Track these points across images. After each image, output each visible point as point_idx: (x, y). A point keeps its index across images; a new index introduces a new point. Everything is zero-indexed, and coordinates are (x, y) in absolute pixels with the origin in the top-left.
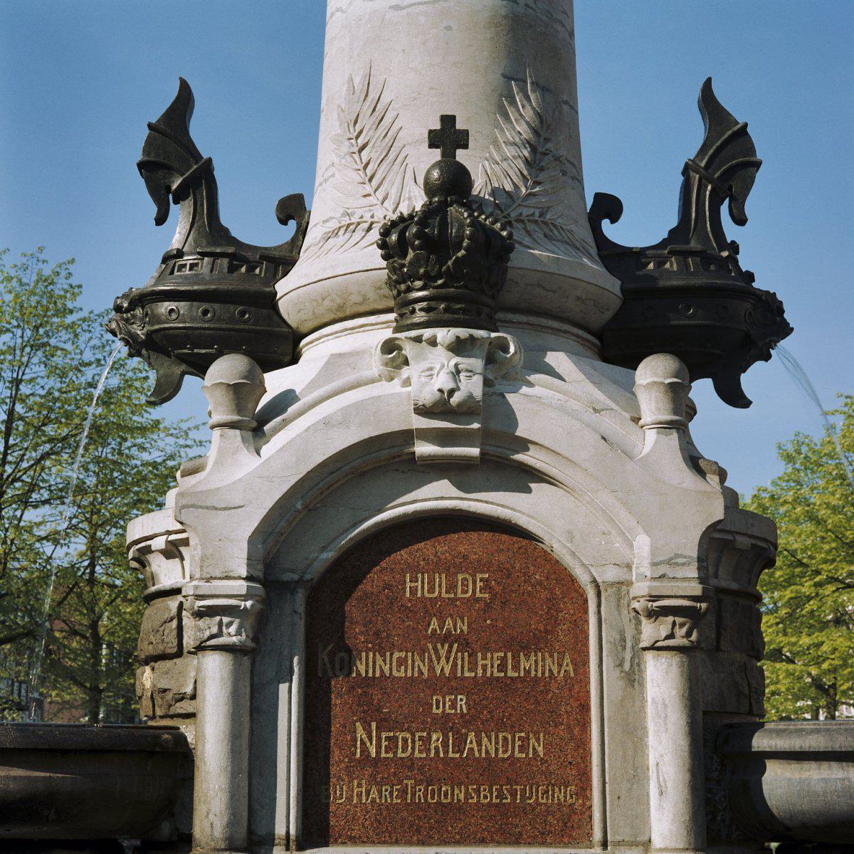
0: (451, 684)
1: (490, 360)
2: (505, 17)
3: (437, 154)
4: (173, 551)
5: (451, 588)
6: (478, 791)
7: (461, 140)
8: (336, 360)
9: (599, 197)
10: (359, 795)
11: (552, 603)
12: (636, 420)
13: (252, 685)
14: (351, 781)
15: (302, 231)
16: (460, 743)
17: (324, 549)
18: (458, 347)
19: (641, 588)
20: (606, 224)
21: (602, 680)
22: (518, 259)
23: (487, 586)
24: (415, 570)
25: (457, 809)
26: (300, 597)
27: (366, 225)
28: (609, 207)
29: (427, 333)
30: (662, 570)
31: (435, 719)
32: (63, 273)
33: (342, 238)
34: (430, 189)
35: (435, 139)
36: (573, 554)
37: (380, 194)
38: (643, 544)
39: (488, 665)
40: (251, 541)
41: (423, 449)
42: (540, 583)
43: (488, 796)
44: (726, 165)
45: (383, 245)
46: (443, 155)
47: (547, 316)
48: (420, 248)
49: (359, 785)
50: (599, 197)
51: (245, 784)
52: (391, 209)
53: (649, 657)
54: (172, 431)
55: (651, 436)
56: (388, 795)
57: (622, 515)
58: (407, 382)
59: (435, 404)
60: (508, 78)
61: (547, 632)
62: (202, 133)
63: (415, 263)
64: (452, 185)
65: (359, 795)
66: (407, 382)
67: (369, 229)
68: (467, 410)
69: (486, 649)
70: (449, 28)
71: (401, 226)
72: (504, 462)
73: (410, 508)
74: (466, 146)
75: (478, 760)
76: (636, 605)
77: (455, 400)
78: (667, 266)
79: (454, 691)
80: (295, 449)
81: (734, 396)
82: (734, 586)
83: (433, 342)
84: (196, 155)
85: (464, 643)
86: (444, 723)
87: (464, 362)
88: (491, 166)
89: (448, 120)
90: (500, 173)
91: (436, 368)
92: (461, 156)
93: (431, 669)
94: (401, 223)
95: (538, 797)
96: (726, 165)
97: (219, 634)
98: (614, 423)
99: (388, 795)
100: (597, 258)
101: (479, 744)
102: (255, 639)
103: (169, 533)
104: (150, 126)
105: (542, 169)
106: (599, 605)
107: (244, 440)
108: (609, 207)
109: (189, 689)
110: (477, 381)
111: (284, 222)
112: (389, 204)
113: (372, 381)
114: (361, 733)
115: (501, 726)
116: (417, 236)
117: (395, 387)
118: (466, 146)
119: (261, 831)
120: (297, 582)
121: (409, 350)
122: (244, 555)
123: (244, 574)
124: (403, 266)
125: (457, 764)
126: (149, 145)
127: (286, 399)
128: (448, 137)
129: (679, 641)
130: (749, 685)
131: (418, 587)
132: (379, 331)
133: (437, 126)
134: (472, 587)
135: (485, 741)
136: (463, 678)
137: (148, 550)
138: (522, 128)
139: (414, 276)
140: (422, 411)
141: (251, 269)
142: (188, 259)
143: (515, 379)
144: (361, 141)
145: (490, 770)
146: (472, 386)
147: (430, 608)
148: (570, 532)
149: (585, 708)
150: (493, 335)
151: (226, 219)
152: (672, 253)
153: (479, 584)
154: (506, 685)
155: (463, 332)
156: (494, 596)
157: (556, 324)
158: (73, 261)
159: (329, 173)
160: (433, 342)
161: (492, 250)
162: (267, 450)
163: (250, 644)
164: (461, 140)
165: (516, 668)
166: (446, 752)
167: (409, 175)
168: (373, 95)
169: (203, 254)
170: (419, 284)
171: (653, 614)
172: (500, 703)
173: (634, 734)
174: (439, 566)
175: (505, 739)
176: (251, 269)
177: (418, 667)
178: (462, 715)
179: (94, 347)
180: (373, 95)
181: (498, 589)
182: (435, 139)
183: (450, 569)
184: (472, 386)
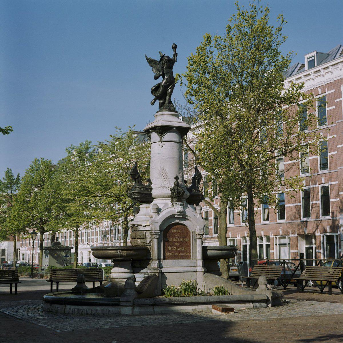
0: (177, 242)
7: (178, 178)
11: (187, 233)
18: (181, 205)
23: (181, 231)
24: (173, 229)
38: (198, 227)
39: (181, 240)
43: (181, 254)
55: (198, 215)
56: (171, 254)
68: (182, 212)
73: (183, 223)
83: (178, 204)
85: (178, 237)
86: (176, 246)
89: (177, 176)
98: (194, 213)
99: (171, 254)
114: (168, 247)
117: (173, 209)
121: (175, 205)
134: (179, 231)
144: (163, 175)
147: (175, 233)
154: (182, 242)
155: (181, 203)
160: (178, 204)
168: (164, 170)
171: (199, 235)
177: (174, 240)
180: (164, 170)
183: (177, 229)
184: (182, 210)
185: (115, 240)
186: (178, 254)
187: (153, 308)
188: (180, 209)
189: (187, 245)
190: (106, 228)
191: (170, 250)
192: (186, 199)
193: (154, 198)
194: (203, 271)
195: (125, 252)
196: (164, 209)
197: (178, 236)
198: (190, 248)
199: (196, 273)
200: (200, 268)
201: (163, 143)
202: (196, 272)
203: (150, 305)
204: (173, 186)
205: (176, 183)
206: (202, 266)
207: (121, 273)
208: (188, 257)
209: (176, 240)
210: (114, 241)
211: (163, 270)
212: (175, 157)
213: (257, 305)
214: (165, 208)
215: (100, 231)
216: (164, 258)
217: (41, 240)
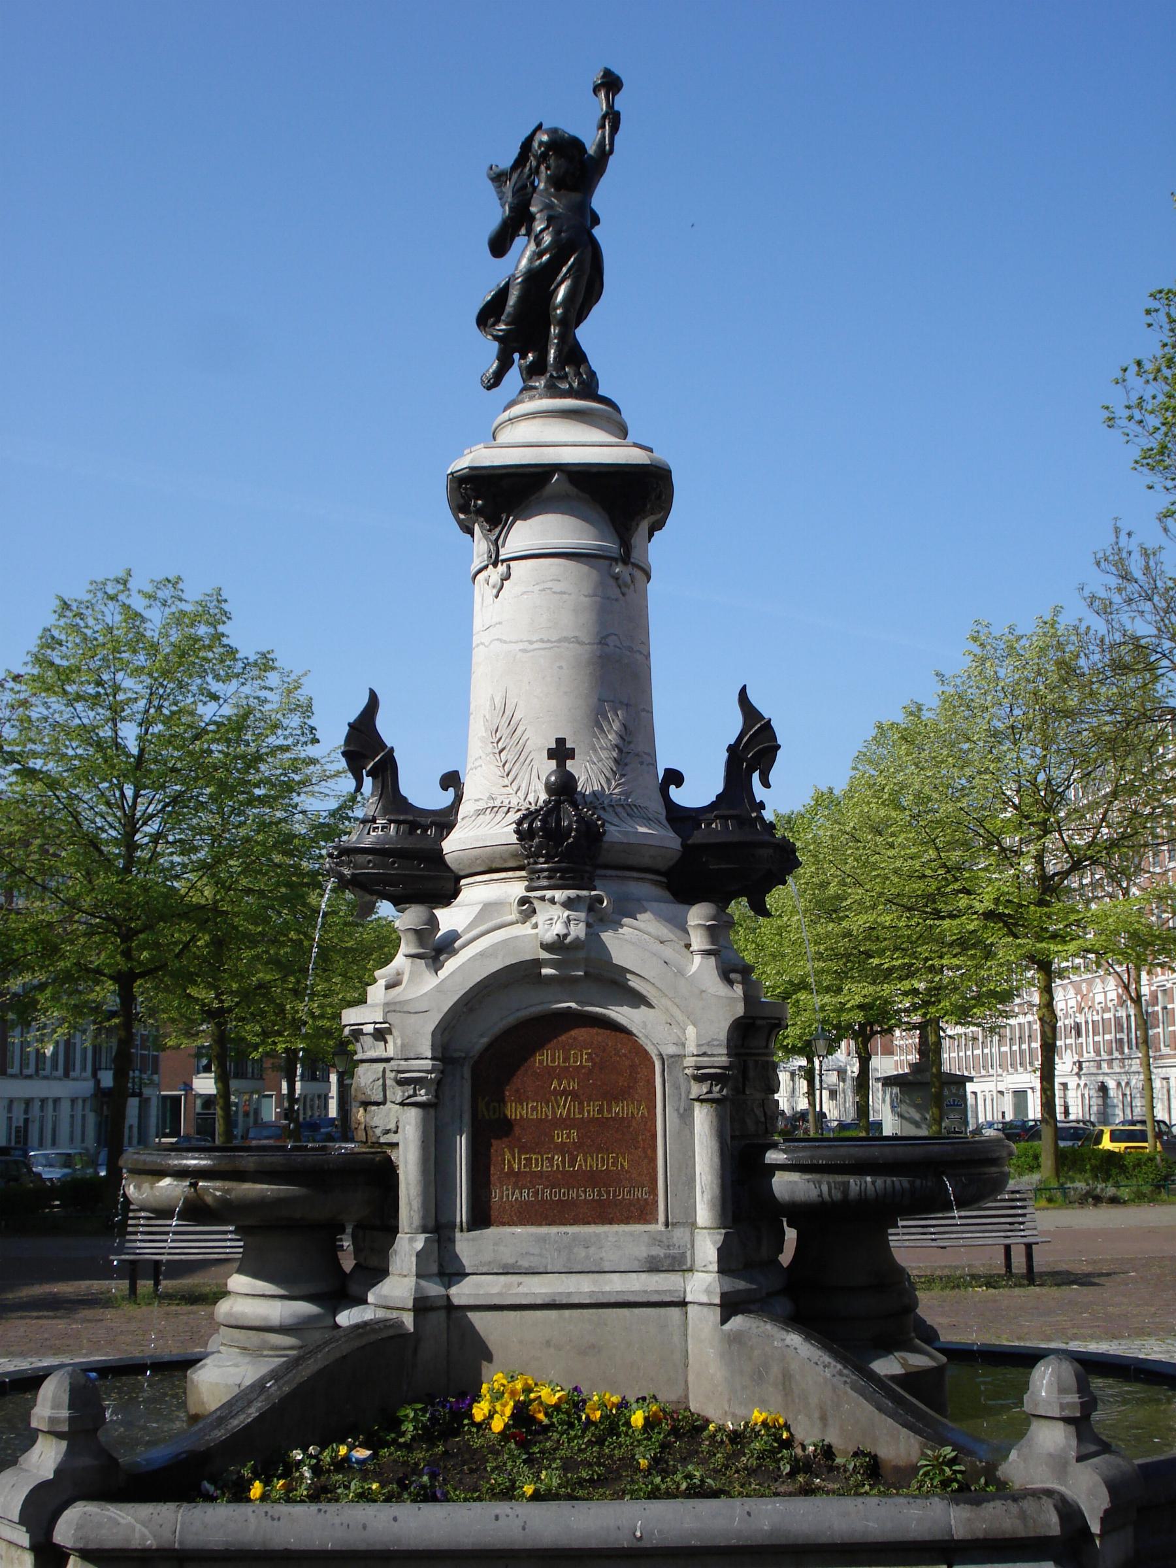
0: (566, 1123)
1: (591, 909)
2: (600, 657)
3: (553, 764)
5: (566, 1059)
6: (585, 1192)
7: (571, 754)
8: (488, 908)
9: (667, 771)
10: (508, 1196)
12: (688, 946)
13: (436, 1126)
14: (501, 1187)
15: (459, 798)
17: (482, 1036)
18: (568, 904)
19: (689, 1061)
20: (672, 788)
21: (664, 1119)
25: (573, 1203)
26: (467, 1072)
27: (505, 809)
28: (674, 777)
29: (549, 894)
30: (703, 1049)
31: (557, 1145)
33: (488, 816)
34: (549, 788)
35: (552, 754)
36: (647, 1037)
37: (515, 786)
39: (591, 1110)
42: (625, 1055)
43: (590, 1195)
44: (755, 749)
45: (517, 832)
46: (558, 766)
47: (630, 865)
48: (541, 837)
49: (507, 1189)
50: (667, 771)
51: (432, 1190)
52: (523, 798)
53: (697, 1104)
55: (698, 959)
57: (680, 1016)
58: (535, 926)
59: (553, 943)
60: (601, 700)
61: (630, 1087)
62: (386, 727)
63: (540, 846)
64: (563, 788)
65: (508, 1196)
66: (535, 926)
67: (508, 811)
68: (577, 944)
69: (590, 1100)
70: (561, 667)
71: (530, 818)
74: (573, 758)
75: (585, 1172)
76: (687, 1071)
77: (569, 940)
78: (714, 826)
81: (760, 909)
84: (383, 745)
85: (575, 1096)
86: (562, 1149)
87: (573, 914)
88: (589, 774)
89: (561, 742)
90: (596, 770)
91: (554, 920)
93: (554, 1113)
94: (530, 816)
95: (624, 1195)
96: (755, 749)
97: (415, 1095)
100: (665, 822)
101: (586, 1161)
102: (437, 1096)
103: (376, 1023)
104: (349, 724)
105: (626, 765)
106: (663, 1071)
107: (427, 965)
108: (674, 777)
109: (392, 1126)
110: (582, 926)
111: (445, 789)
112: (521, 794)
113: (512, 924)
114: (507, 1156)
115: (599, 1150)
116: (541, 829)
117: (525, 930)
118: (573, 758)
119: (443, 1220)
120: (464, 1058)
122: (429, 1043)
123: (430, 1056)
124: (531, 846)
125: (573, 1174)
126: (349, 739)
127: (453, 936)
128: (560, 752)
129: (715, 1095)
130: (765, 1114)
132: (515, 889)
133: (554, 746)
135: (589, 1159)
136: (574, 1119)
137: (361, 1032)
139: (537, 855)
140: (546, 947)
145: (592, 1179)
146: (578, 931)
147: (552, 1073)
148: (644, 1022)
149: (654, 1136)
150: (593, 893)
151: (404, 790)
152: (717, 817)
153: (585, 1057)
154: (602, 1123)
155: (572, 893)
156: (594, 1064)
157: (635, 874)
159: (477, 764)
161: (591, 834)
162: (443, 973)
163: (434, 1100)
165: (610, 1111)
166: (564, 1167)
167: (534, 773)
168: (508, 713)
169: (391, 821)
170: (542, 860)
175: (603, 1158)
177: (545, 1112)
178: (574, 1143)
180: (508, 713)
181: (597, 1060)
182: (552, 754)
184: (578, 931)
185: (1130, 1048)
186: (573, 1194)
188: (558, 928)
189: (638, 1138)
190: (1103, 1012)
193: (459, 878)
194: (717, 1301)
198: (654, 1160)
200: (703, 1283)
201: (501, 568)
205: (553, 779)
206: (715, 1267)
207: (250, 1300)
208: (643, 1212)
209: (562, 1112)
210: (1126, 1050)
211: (461, 1293)
212: (566, 639)
215: (1087, 1022)
216: (481, 1218)
217: (860, 1057)
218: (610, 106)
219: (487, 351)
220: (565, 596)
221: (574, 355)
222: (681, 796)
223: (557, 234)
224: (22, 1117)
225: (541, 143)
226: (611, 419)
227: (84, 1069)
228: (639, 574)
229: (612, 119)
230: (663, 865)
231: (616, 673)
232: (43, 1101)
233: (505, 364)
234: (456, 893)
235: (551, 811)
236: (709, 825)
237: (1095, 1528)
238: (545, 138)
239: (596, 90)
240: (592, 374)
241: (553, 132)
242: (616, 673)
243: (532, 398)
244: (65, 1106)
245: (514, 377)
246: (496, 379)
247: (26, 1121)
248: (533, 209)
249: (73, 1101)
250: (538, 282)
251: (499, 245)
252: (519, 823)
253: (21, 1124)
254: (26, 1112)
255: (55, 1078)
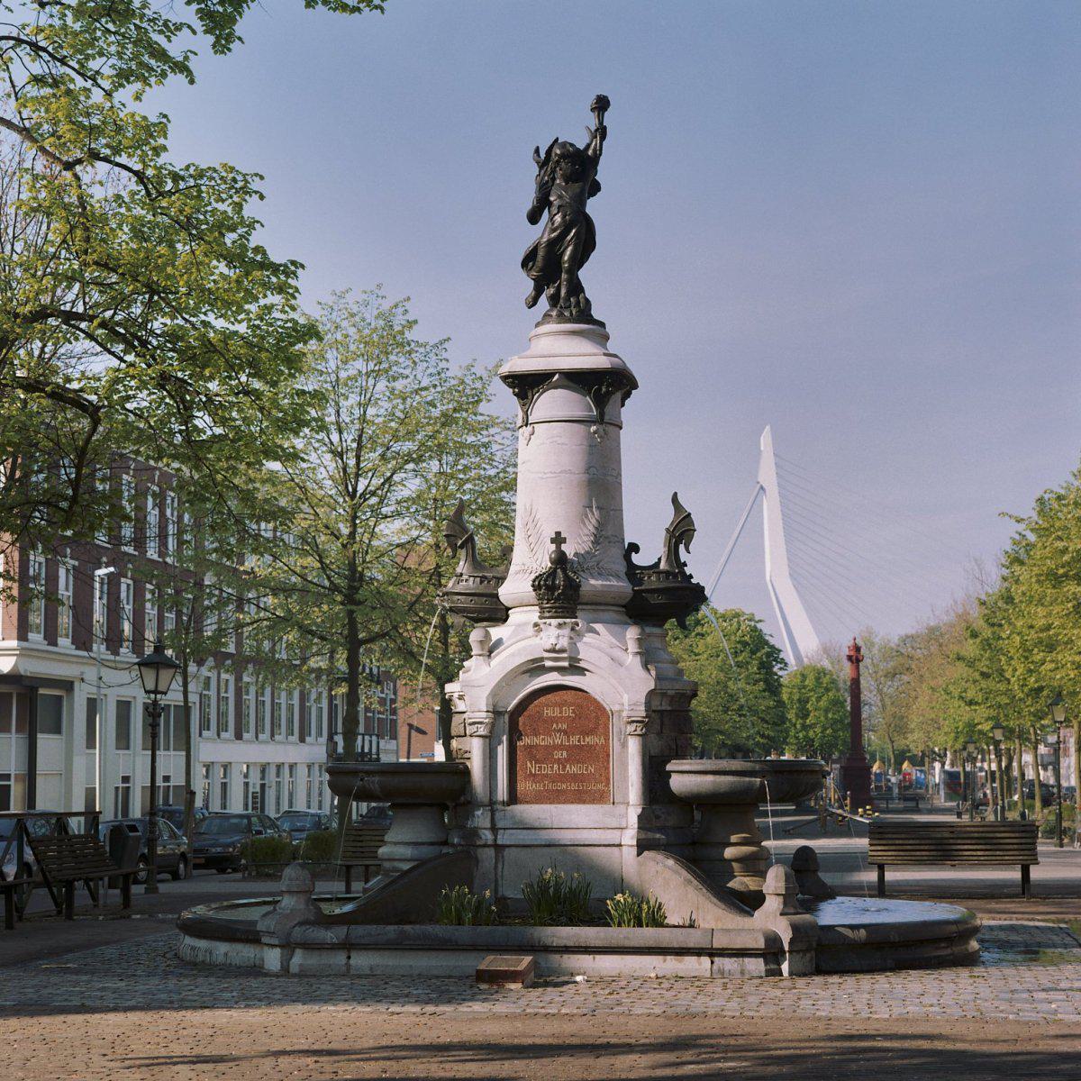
0: (560, 747)
3: (554, 545)
4: (461, 698)
7: (564, 540)
9: (630, 544)
11: (597, 718)
12: (627, 650)
16: (564, 767)
19: (625, 714)
21: (615, 745)
22: (584, 589)
23: (574, 712)
24: (548, 706)
25: (564, 792)
26: (507, 717)
28: (634, 548)
32: (400, 310)
35: (553, 541)
39: (574, 740)
40: (487, 699)
41: (548, 664)
43: (574, 787)
44: (681, 531)
45: (533, 586)
50: (630, 544)
51: (488, 782)
54: (508, 426)
55: (631, 656)
57: (621, 689)
64: (560, 560)
69: (573, 734)
72: (575, 668)
79: (562, 750)
80: (507, 660)
82: (669, 708)
85: (565, 732)
86: (559, 761)
89: (558, 534)
91: (554, 634)
92: (564, 547)
96: (681, 531)
98: (618, 653)
100: (625, 578)
102: (490, 732)
108: (634, 548)
114: (529, 765)
117: (537, 640)
127: (499, 642)
128: (558, 539)
129: (639, 732)
131: (548, 712)
134: (568, 712)
138: (591, 528)
141: (489, 582)
142: (465, 577)
143: (580, 635)
147: (553, 720)
149: (608, 755)
155: (561, 621)
158: (409, 299)
161: (573, 587)
164: (564, 540)
172: (578, 754)
173: (625, 765)
174: (556, 704)
176: (489, 582)
179: (431, 375)
182: (553, 541)
183: (561, 706)
187: (349, 958)
188: (553, 641)
189: (601, 757)
191: (535, 775)
192: (508, 609)
193: (508, 609)
194: (635, 843)
195: (376, 779)
196: (511, 641)
197: (565, 726)
199: (621, 851)
201: (529, 428)
202: (620, 845)
203: (334, 947)
204: (546, 564)
206: (636, 826)
209: (558, 741)
212: (565, 472)
213: (728, 964)
214: (514, 640)
218: (601, 123)
219: (528, 286)
220: (564, 447)
221: (576, 288)
222: (637, 559)
223: (564, 217)
224: (259, 782)
225: (556, 154)
226: (598, 333)
227: (320, 734)
228: (611, 428)
229: (602, 132)
230: (624, 602)
231: (601, 484)
232: (279, 767)
233: (538, 291)
234: (508, 617)
235: (551, 574)
236: (649, 577)
237: (787, 948)
238: (558, 152)
239: (593, 110)
240: (588, 302)
241: (564, 145)
242: (601, 484)
243: (548, 323)
244: (302, 772)
245: (543, 302)
246: (533, 302)
247: (263, 786)
248: (552, 199)
249: (309, 767)
250: (554, 246)
251: (534, 217)
252: (534, 581)
253: (258, 789)
254: (263, 778)
255: (292, 743)
